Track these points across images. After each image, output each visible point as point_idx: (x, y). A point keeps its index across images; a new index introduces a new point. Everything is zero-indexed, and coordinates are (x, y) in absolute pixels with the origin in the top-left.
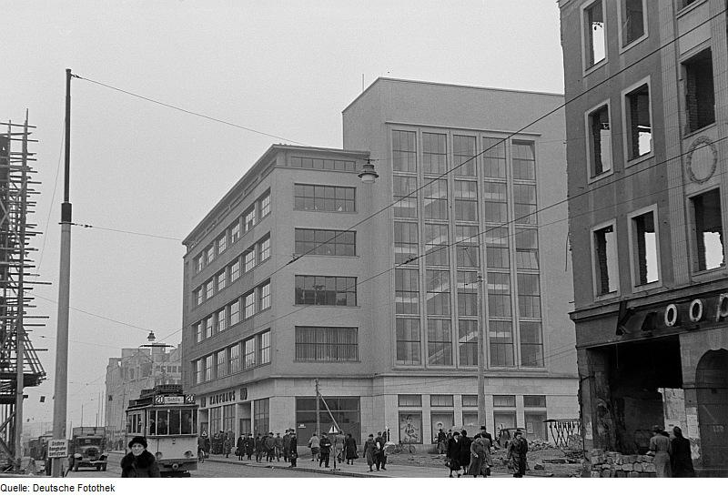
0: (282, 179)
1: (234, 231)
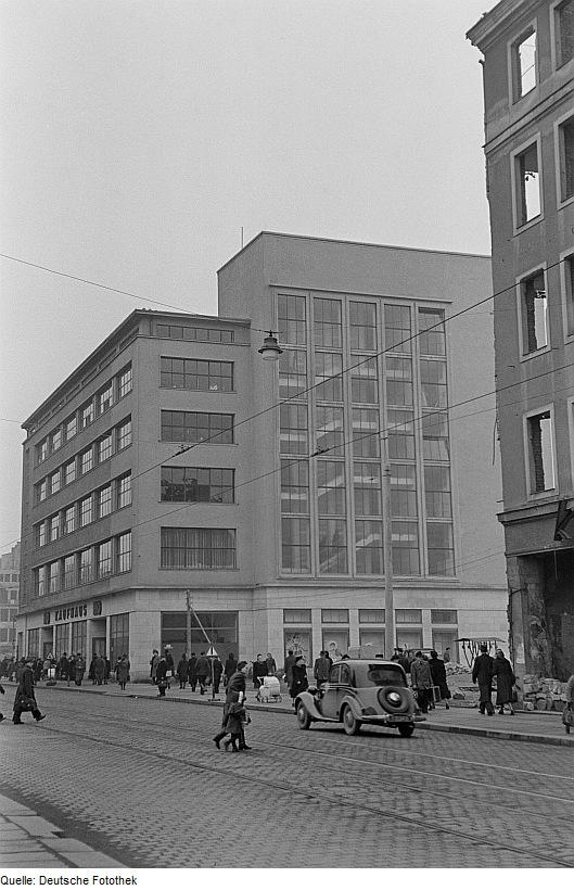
0: (146, 352)
1: (86, 413)
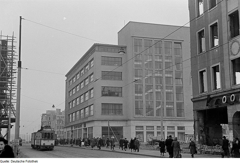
0: (97, 55)
1: (82, 72)
